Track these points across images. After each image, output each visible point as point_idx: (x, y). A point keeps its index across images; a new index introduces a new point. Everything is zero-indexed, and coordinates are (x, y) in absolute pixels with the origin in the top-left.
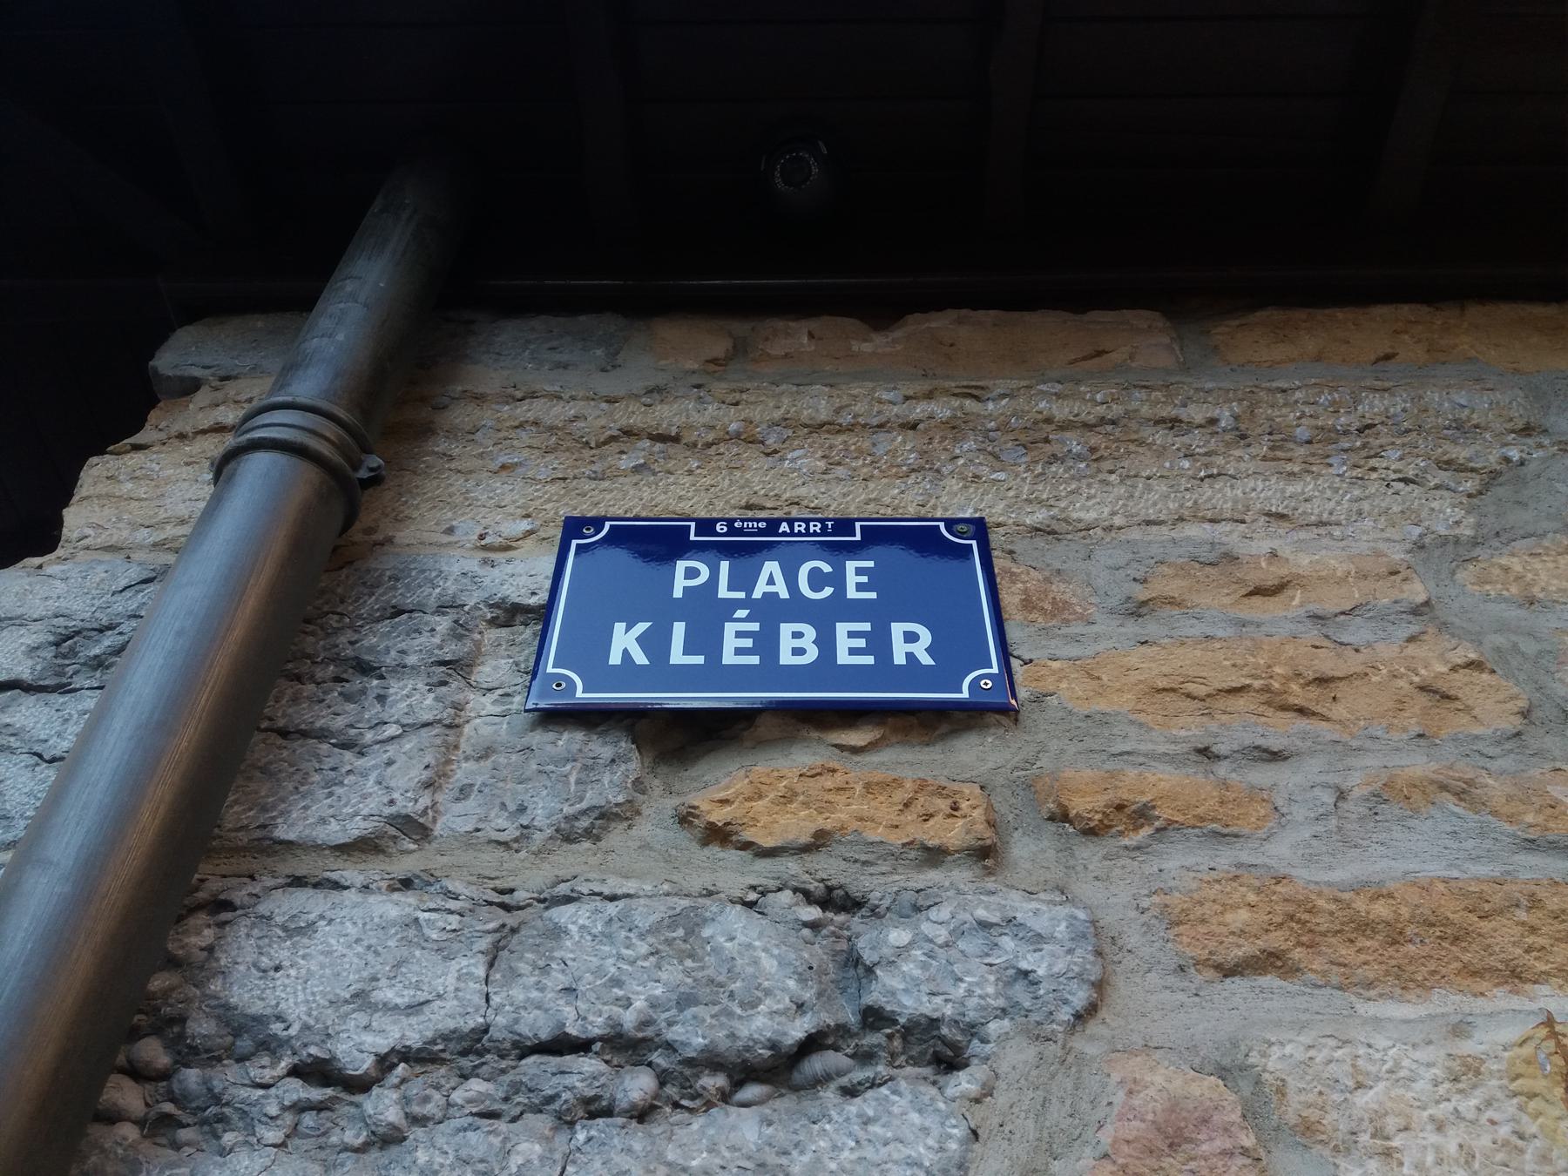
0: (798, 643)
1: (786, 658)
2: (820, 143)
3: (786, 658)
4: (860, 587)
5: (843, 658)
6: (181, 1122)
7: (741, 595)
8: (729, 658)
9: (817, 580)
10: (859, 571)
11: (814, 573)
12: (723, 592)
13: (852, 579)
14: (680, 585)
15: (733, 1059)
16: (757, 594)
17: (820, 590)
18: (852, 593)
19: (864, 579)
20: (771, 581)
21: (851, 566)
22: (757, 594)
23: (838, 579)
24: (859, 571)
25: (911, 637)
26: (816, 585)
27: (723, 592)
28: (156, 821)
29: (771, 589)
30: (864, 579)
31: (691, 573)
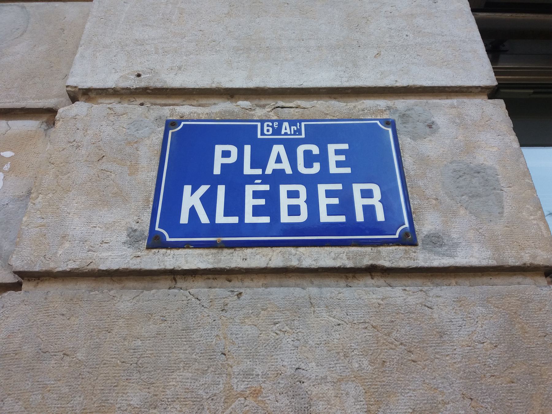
0: (294, 202)
1: (285, 218)
2: (298, 123)
3: (285, 218)
4: (339, 164)
5: (324, 218)
6: (18, 275)
7: (259, 172)
8: (249, 218)
9: (309, 159)
10: (338, 152)
11: (307, 153)
12: (248, 170)
13: (333, 159)
14: (219, 161)
15: (262, 279)
16: (269, 171)
17: (311, 166)
18: (333, 169)
19: (342, 158)
20: (279, 160)
21: (332, 148)
22: (269, 171)
23: (323, 158)
24: (338, 152)
25: (367, 194)
26: (308, 164)
27: (248, 170)
28: (8, 104)
29: (279, 166)
30: (342, 158)
31: (226, 154)
